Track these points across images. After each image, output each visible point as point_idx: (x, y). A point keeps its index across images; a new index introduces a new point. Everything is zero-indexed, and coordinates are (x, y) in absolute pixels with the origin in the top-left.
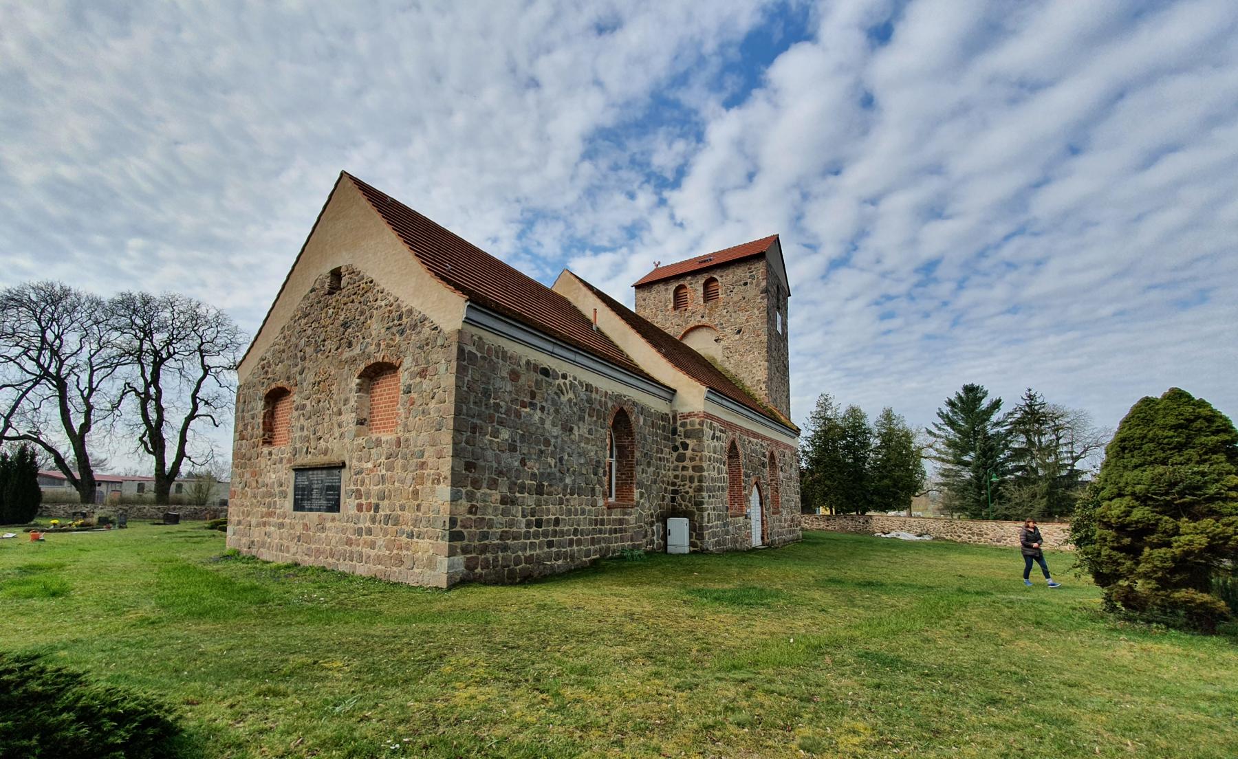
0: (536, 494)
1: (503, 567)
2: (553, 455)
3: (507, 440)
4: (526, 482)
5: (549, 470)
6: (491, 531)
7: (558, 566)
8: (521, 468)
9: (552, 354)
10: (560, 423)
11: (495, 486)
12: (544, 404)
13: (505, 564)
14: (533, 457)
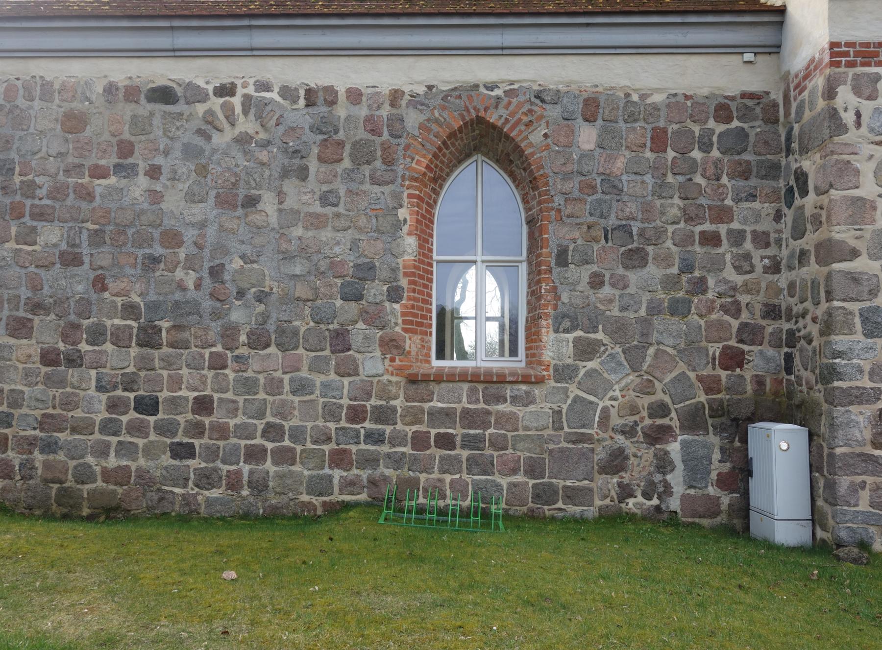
0: (140, 345)
1: (46, 481)
2: (191, 264)
3: (55, 245)
4: (109, 323)
5: (178, 296)
6: (17, 412)
7: (209, 502)
8: (94, 296)
9: (175, 53)
10: (213, 193)
11: (24, 331)
12: (159, 160)
13: (50, 476)
14: (130, 271)
